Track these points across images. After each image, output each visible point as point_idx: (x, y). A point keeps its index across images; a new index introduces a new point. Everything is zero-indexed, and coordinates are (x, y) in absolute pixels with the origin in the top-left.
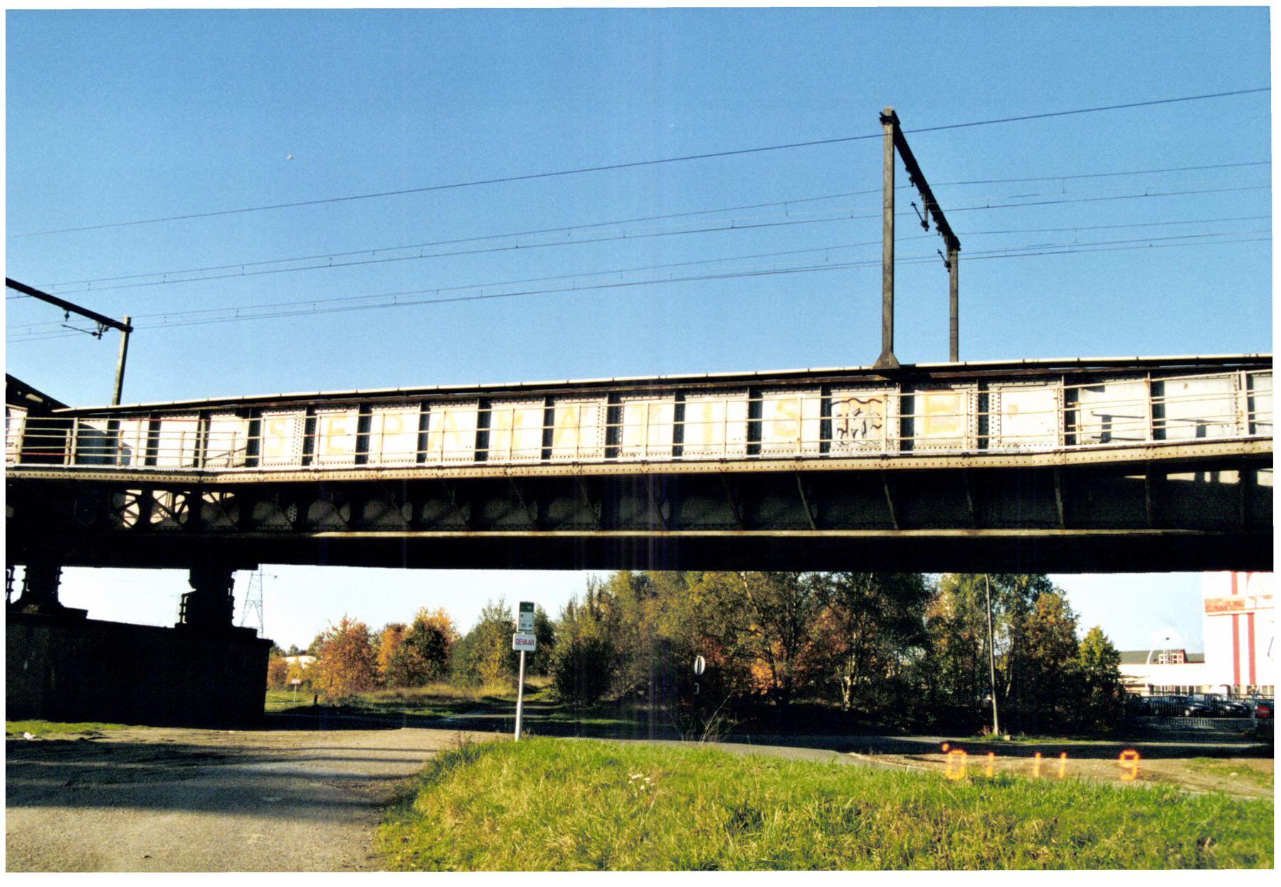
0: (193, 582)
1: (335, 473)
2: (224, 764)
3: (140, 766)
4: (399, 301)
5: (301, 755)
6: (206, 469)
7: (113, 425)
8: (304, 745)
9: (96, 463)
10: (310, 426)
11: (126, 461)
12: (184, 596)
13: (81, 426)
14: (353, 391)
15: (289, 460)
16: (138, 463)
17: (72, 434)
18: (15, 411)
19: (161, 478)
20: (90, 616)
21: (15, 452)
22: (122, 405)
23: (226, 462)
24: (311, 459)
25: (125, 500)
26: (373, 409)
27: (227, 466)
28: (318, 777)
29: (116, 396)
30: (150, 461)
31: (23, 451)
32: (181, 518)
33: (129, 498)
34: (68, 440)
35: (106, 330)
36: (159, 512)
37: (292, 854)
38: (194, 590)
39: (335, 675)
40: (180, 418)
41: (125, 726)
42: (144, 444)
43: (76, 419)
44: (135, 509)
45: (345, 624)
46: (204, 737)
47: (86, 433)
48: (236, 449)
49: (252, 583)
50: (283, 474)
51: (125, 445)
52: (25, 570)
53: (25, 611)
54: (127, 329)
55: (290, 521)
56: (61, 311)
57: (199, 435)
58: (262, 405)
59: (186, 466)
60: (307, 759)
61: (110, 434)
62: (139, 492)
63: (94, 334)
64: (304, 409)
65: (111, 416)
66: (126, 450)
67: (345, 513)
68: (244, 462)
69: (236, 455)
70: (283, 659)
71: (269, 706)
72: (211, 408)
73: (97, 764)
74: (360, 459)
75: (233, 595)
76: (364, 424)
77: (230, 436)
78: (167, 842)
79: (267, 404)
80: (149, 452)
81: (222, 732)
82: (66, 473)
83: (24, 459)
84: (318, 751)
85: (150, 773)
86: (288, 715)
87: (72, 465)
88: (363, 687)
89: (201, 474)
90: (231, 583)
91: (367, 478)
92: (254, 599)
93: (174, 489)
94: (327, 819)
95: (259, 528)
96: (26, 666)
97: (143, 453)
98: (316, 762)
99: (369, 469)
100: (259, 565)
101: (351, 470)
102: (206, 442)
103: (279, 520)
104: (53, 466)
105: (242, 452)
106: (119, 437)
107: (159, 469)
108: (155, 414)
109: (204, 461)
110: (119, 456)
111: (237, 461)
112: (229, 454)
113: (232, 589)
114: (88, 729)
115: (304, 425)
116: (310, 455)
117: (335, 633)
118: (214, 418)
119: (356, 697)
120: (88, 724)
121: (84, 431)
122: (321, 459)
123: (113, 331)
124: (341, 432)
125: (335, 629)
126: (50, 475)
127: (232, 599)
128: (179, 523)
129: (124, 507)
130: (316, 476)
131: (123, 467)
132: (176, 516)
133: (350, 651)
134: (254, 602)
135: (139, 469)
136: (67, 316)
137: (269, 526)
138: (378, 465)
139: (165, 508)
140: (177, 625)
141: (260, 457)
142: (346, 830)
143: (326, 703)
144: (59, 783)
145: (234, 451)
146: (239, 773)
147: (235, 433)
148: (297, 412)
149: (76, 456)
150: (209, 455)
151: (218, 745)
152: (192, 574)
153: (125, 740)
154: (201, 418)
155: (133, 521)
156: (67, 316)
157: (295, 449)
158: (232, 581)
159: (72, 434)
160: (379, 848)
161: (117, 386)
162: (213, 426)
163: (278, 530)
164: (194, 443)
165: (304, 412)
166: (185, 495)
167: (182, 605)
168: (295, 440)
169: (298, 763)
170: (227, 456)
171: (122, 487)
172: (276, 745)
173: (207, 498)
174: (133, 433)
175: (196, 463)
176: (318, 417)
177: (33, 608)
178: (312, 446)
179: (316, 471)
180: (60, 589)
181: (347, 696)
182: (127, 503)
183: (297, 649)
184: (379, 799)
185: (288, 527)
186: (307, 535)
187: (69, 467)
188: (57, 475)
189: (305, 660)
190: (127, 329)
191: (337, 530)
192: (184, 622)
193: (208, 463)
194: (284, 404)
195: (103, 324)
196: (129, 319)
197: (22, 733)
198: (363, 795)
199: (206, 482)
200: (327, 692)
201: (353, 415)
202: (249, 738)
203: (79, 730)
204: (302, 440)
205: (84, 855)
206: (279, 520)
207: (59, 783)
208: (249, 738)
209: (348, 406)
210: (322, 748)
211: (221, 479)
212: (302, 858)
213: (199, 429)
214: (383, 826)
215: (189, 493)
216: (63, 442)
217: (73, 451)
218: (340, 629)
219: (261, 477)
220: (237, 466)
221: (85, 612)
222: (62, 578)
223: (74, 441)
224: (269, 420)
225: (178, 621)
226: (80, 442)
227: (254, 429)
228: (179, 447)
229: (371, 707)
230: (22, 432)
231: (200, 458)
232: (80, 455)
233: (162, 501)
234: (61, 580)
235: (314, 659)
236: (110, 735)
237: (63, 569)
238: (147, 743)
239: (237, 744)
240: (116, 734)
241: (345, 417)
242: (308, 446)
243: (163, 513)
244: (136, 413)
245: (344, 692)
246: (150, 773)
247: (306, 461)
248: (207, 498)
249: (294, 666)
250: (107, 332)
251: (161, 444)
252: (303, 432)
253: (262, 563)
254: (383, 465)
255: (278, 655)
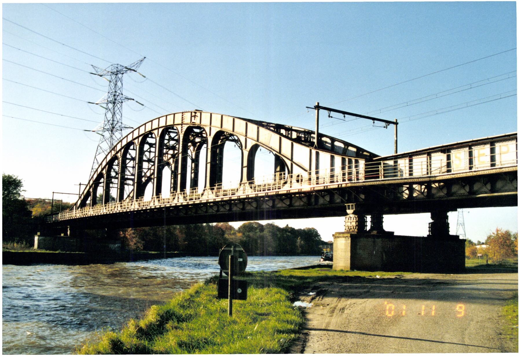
0: (432, 218)
1: (482, 171)
2: (448, 285)
3: (417, 286)
4: (502, 97)
5: (478, 282)
6: (432, 175)
7: (396, 162)
8: (479, 279)
9: (391, 177)
10: (471, 154)
11: (402, 175)
12: (429, 224)
13: (384, 164)
14: (486, 137)
15: (463, 168)
16: (406, 175)
17: (381, 167)
18: (361, 161)
19: (415, 180)
20: (395, 234)
21: (362, 176)
22: (398, 153)
23: (439, 171)
24: (472, 167)
25: (403, 189)
26: (496, 144)
27: (440, 173)
28: (484, 290)
29: (395, 149)
30: (411, 174)
31: (365, 175)
32: (424, 193)
33: (404, 189)
34: (380, 170)
35: (389, 125)
36: (416, 192)
37: (470, 314)
38: (433, 221)
39: (496, 252)
40: (420, 156)
41: (412, 273)
42: (408, 168)
43: (382, 162)
44: (407, 192)
45: (497, 231)
46: (441, 277)
47: (386, 167)
48: (443, 166)
49: (459, 216)
50: (461, 174)
51: (400, 169)
52: (371, 217)
53: (372, 233)
54: (396, 123)
55: (467, 191)
56: (372, 121)
57: (427, 162)
58: (451, 147)
59: (424, 175)
60: (480, 284)
61: (395, 166)
62: (408, 186)
63: (384, 127)
64: (467, 147)
65: (395, 159)
66: (401, 171)
67: (489, 186)
68: (446, 171)
69: (443, 168)
70: (475, 246)
71: (467, 265)
72: (431, 151)
73: (402, 286)
74: (493, 165)
75: (449, 222)
76: (492, 151)
77: (440, 161)
78: (426, 310)
79: (452, 147)
80: (410, 171)
81: (448, 275)
82: (381, 182)
83: (366, 178)
84: (485, 281)
85: (421, 289)
86: (475, 268)
87: (383, 179)
88: (509, 256)
89: (430, 177)
90: (447, 217)
91: (496, 172)
92: (461, 222)
93: (421, 183)
94: (485, 303)
95: (455, 195)
96: (374, 253)
97: (408, 172)
98: (483, 285)
99: (496, 169)
100: (458, 209)
101: (489, 170)
102: (430, 165)
103: (462, 191)
104: (376, 180)
105: (445, 167)
106: (398, 167)
107: (414, 177)
108: (410, 156)
109: (431, 172)
110: (399, 174)
111: (443, 171)
112: (440, 168)
113: (448, 219)
114: (398, 274)
115: (468, 153)
116: (472, 166)
117: (493, 235)
118: (433, 155)
119: (505, 260)
120: (398, 272)
121: (386, 166)
122: (476, 166)
123: (392, 125)
124: (483, 155)
125: (494, 233)
126: (375, 183)
127: (448, 224)
128: (424, 195)
129: (403, 192)
130: (475, 174)
131: (401, 178)
132: (422, 193)
133: (501, 242)
134: (461, 223)
135: (407, 178)
136: (374, 122)
137: (459, 194)
138: (500, 166)
139: (418, 191)
140: (428, 235)
141: (452, 168)
142: (492, 307)
143: (492, 263)
144: (389, 292)
145: (442, 167)
146: (452, 289)
147: (441, 160)
148: (465, 149)
149: (383, 175)
150: (432, 170)
151: (445, 279)
152: (432, 215)
153: (412, 278)
154: (428, 155)
155: (407, 196)
156: (374, 122)
157: (465, 164)
158: (448, 216)
159: (381, 167)
160: (504, 313)
161: (395, 145)
162: (433, 158)
163: (461, 195)
164: (426, 166)
165: (468, 148)
166: (425, 185)
167: (429, 227)
168: (465, 160)
169: (476, 285)
170: (439, 169)
171: (401, 185)
172: (468, 279)
173: (433, 185)
174: (403, 164)
175: (428, 174)
176: (473, 150)
177: (375, 232)
178: (472, 162)
179: (475, 171)
180: (384, 224)
181: (501, 260)
182: (404, 190)
183: (480, 242)
184: (506, 297)
185: (466, 194)
186: (474, 196)
187: (381, 180)
188: (378, 183)
189: (484, 246)
190: (396, 123)
191: (486, 193)
192: (430, 234)
193: (432, 172)
194: (459, 146)
195: (387, 123)
196: (396, 120)
197: (376, 276)
198: (500, 296)
199: (432, 180)
200: (493, 259)
201: (488, 147)
202: (458, 276)
203: (395, 275)
204: (468, 160)
205: (399, 312)
206: (462, 191)
207: (389, 292)
208: (458, 276)
209: (485, 144)
210: (487, 280)
211: (438, 178)
212: (474, 316)
213: (427, 160)
214: (506, 306)
215: (426, 184)
216: (378, 171)
217: (382, 174)
218: (496, 233)
219: (453, 176)
220: (444, 173)
221: (393, 233)
222: (384, 220)
223: (382, 170)
224: (454, 153)
225: (428, 234)
226: (384, 170)
227: (449, 158)
228: (421, 168)
229: (511, 264)
230: (364, 169)
231: (429, 171)
232: (385, 175)
233: (417, 188)
234: (383, 221)
235: (488, 246)
236: (406, 276)
237: (384, 216)
238: (420, 279)
239: (453, 279)
240: (408, 276)
241: (484, 149)
242: (471, 162)
243: (417, 192)
244: (403, 156)
245: (500, 258)
246: (421, 289)
247: (471, 168)
248: (433, 185)
249: (480, 249)
250: (389, 126)
251: (414, 168)
252: (468, 156)
253: (459, 208)
254: (502, 167)
255: (472, 245)
